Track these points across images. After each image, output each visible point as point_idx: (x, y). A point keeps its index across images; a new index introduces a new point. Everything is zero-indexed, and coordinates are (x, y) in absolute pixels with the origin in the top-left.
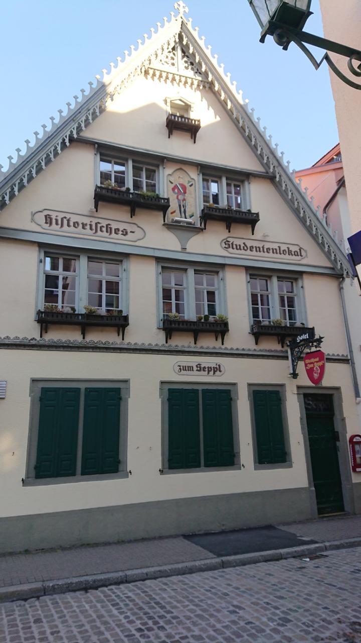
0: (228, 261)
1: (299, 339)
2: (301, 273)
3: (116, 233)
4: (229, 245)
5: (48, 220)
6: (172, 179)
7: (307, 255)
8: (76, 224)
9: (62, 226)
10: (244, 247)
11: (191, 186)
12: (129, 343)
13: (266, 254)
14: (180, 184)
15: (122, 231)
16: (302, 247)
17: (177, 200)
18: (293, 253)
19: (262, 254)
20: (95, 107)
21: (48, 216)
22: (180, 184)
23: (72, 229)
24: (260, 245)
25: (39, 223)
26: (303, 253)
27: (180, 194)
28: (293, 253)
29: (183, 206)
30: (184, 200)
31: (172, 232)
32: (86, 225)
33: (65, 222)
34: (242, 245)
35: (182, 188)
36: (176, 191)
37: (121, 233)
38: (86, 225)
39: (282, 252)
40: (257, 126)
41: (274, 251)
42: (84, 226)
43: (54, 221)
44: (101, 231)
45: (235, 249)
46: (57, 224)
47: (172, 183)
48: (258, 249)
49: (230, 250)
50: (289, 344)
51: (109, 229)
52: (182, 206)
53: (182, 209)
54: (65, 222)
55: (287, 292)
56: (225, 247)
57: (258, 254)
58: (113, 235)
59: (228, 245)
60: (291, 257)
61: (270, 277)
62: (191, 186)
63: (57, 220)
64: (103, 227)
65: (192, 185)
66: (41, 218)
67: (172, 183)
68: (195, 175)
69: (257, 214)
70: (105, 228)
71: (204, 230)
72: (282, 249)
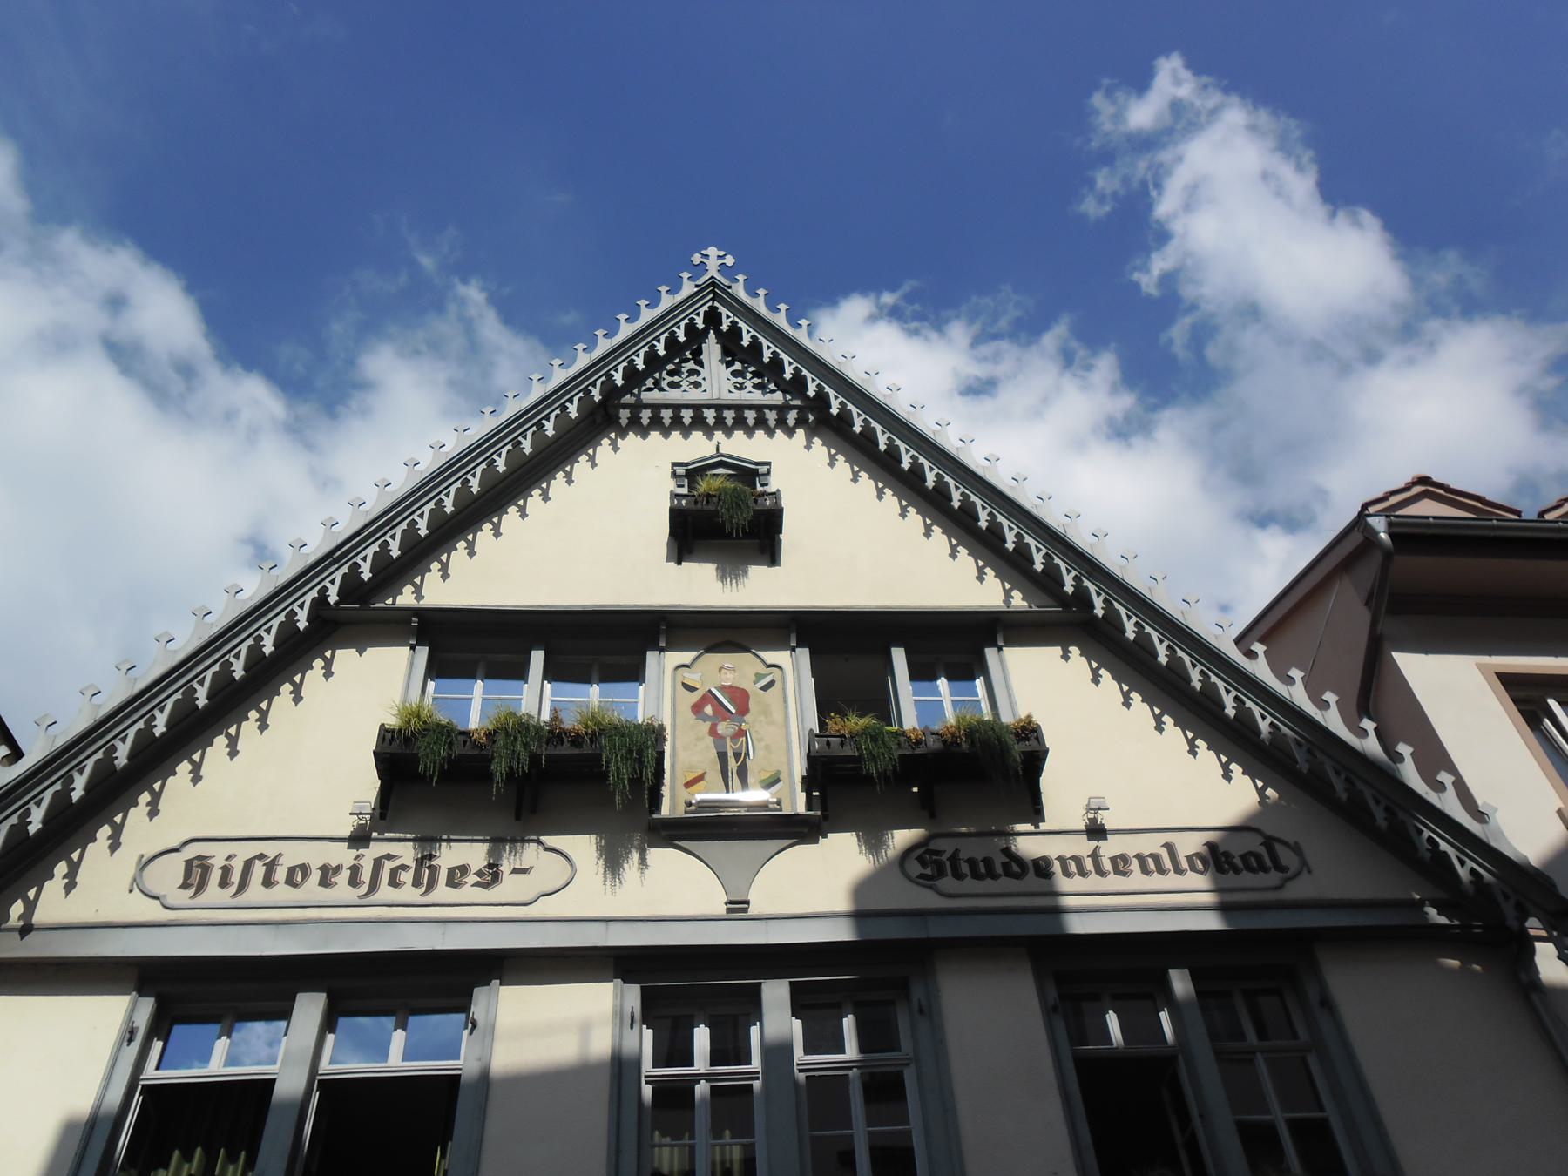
0: (938, 930)
3: (290, 881)
5: (196, 874)
6: (691, 677)
7: (1304, 864)
8: (298, 874)
9: (243, 885)
10: (1005, 866)
11: (765, 688)
13: (1113, 882)
14: (722, 689)
16: (1269, 831)
17: (710, 740)
18: (1238, 861)
20: (415, 517)
21: (196, 863)
22: (722, 689)
23: (282, 892)
25: (155, 892)
26: (1286, 857)
27: (724, 719)
28: (1238, 861)
29: (737, 755)
32: (337, 869)
33: (259, 870)
35: (732, 701)
36: (708, 710)
38: (337, 869)
39: (1184, 864)
42: (327, 875)
43: (216, 875)
44: (394, 882)
46: (224, 883)
49: (948, 883)
52: (730, 754)
54: (259, 870)
56: (922, 876)
62: (765, 688)
63: (226, 871)
64: (404, 867)
65: (772, 683)
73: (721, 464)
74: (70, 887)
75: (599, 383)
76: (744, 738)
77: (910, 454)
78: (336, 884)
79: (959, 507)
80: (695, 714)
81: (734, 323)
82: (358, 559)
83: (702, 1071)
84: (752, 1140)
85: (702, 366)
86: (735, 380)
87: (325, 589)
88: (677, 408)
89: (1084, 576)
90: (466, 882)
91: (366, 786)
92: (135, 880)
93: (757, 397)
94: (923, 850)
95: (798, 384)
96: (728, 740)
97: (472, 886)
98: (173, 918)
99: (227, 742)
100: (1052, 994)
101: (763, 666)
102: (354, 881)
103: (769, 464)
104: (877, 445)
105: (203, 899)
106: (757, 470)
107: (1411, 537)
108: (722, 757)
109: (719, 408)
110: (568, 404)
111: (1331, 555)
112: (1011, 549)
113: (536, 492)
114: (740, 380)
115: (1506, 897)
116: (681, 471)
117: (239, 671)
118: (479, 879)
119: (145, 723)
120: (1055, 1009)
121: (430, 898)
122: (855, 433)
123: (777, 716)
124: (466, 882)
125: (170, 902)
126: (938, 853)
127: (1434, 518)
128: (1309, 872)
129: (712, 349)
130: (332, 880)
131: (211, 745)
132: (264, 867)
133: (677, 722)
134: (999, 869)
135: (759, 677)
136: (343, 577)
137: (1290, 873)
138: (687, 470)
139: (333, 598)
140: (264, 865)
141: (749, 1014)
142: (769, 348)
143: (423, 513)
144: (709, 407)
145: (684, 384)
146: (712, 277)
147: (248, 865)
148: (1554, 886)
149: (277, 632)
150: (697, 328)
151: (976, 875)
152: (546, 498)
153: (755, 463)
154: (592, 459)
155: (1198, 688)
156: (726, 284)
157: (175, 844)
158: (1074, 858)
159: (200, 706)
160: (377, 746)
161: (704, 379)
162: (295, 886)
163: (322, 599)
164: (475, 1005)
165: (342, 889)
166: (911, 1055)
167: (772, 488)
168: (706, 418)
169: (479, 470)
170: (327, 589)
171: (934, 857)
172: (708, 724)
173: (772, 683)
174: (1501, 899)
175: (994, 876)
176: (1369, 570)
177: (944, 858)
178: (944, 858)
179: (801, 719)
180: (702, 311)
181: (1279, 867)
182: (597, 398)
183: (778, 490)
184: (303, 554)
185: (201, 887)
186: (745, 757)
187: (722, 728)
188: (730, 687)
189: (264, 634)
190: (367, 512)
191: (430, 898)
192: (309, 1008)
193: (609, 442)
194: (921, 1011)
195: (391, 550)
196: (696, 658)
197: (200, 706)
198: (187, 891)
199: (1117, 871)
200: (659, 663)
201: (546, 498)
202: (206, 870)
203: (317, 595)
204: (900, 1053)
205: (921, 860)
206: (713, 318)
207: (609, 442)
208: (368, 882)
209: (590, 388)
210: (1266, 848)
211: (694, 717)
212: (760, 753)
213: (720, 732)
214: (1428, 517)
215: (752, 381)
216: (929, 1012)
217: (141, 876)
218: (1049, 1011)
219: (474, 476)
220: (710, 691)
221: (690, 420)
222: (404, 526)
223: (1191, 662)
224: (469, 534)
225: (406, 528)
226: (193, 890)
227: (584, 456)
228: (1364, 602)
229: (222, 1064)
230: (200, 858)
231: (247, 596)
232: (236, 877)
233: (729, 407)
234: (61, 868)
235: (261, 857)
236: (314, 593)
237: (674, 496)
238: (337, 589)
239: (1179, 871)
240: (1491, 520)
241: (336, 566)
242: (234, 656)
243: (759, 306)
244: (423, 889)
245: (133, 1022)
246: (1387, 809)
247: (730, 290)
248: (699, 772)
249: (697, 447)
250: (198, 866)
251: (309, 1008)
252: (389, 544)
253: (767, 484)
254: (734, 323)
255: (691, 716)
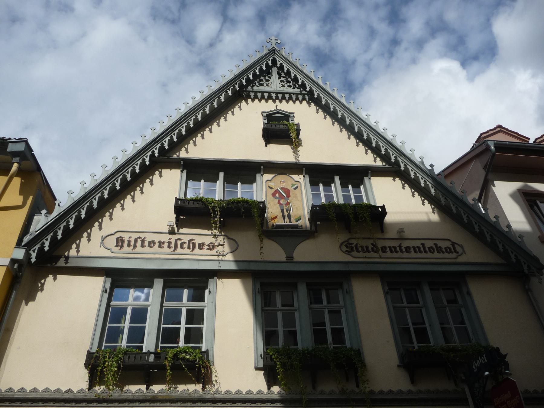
0: (352, 268)
1: (476, 365)
2: (463, 275)
3: (149, 246)
4: (352, 248)
5: (120, 242)
6: (271, 184)
7: (464, 251)
8: (151, 244)
9: (135, 247)
10: (372, 249)
11: (295, 189)
12: (217, 392)
13: (406, 255)
14: (281, 188)
15: (208, 245)
16: (454, 240)
17: (278, 205)
18: (444, 250)
19: (399, 255)
20: (181, 128)
21: (119, 239)
22: (281, 188)
23: (147, 249)
24: (396, 244)
25: (108, 247)
26: (458, 249)
27: (282, 199)
28: (444, 250)
29: (287, 211)
30: (288, 203)
31: (273, 240)
32: (164, 243)
33: (139, 242)
34: (371, 247)
35: (285, 192)
36: (277, 195)
37: (206, 247)
38: (164, 243)
39: (427, 250)
40: (367, 122)
41: (417, 250)
42: (161, 244)
43: (126, 243)
44: (182, 247)
45: (399, 253)
46: (129, 245)
47: (271, 188)
48: (393, 249)
49: (355, 253)
50: (463, 378)
51: (191, 245)
52: (285, 210)
53: (286, 214)
54: (139, 242)
55: (283, 306)
56: (346, 251)
57: (395, 255)
58: (197, 251)
59: (349, 248)
60: (441, 255)
61: (295, 286)
62: (295, 189)
63: (129, 242)
64: (185, 243)
65: (297, 187)
66: (111, 242)
67: (271, 188)
68: (302, 180)
69: (383, 207)
70: (187, 244)
71: (316, 234)
72: (427, 246)
73: (278, 113)
74: (89, 240)
75: (238, 83)
76: (289, 205)
77: (341, 112)
78: (164, 247)
79: (357, 131)
80: (273, 197)
81: (281, 64)
82: (163, 142)
83: (279, 308)
84: (296, 329)
85: (271, 79)
86: (281, 84)
87: (154, 151)
88: (263, 93)
89: (398, 156)
90: (204, 248)
91: (172, 217)
92: (101, 243)
93: (290, 90)
94: (347, 243)
95: (303, 86)
96: (284, 205)
97: (206, 249)
98: (114, 256)
99: (131, 197)
100: (387, 288)
101: (294, 181)
102: (169, 247)
103: (294, 113)
104: (330, 109)
105: (122, 250)
106: (290, 115)
107: (501, 147)
108: (282, 211)
109: (277, 93)
110: (228, 90)
111: (469, 155)
112: (374, 146)
113: (215, 124)
114: (283, 84)
115: (525, 263)
116: (265, 115)
117: (95, 205)
118: (208, 247)
119: (101, 194)
120: (387, 293)
121: (193, 253)
122: (323, 104)
123: (299, 198)
124: (204, 248)
125: (113, 251)
126: (352, 244)
127: (508, 142)
128: (465, 254)
129: (275, 70)
130: (163, 246)
131: (126, 198)
132: (141, 241)
133: (267, 199)
134: (370, 250)
135: (293, 185)
136: (99, 197)
137: (459, 254)
138: (267, 114)
139: (157, 155)
140: (141, 240)
141: (276, 291)
142: (293, 73)
143: (138, 163)
144: (273, 93)
145: (265, 84)
146: (273, 47)
147: (136, 240)
148: (539, 260)
149: (75, 219)
150: (250, 79)
151: (363, 251)
152: (211, 131)
153: (289, 113)
154: (240, 107)
155: (434, 195)
156: (278, 50)
157: (112, 233)
158: (393, 247)
159: (106, 198)
160: (175, 204)
161: (271, 83)
162: (151, 247)
163: (153, 155)
164: (210, 286)
165: (165, 249)
166: (343, 305)
167: (296, 122)
168: (272, 97)
169: (200, 113)
170: (135, 168)
171: (350, 245)
172: (278, 200)
173: (297, 187)
174: (523, 264)
175: (369, 252)
176: (486, 158)
177: (353, 246)
178: (353, 246)
179: (307, 200)
180: (270, 59)
181: (456, 252)
182: (238, 89)
183: (299, 123)
184: (145, 139)
185: (122, 247)
186: (290, 211)
187: (282, 201)
188: (284, 188)
189: (135, 166)
190: (165, 126)
191: (193, 253)
192: (159, 284)
193: (217, 124)
194: (347, 292)
195: (190, 125)
196: (274, 177)
197: (106, 198)
198: (118, 248)
199: (430, 252)
200: (261, 179)
201: (211, 131)
202: (123, 241)
203: (151, 153)
204: (339, 305)
205: (346, 246)
206: (274, 62)
207: (217, 124)
208: (175, 246)
209: (235, 85)
210: (452, 246)
211: (273, 197)
212: (295, 210)
213: (281, 203)
214: (507, 142)
215: (287, 84)
216: (349, 293)
217: (103, 243)
218: (386, 294)
219: (199, 114)
220: (277, 189)
221: (267, 97)
222: (177, 131)
223: (432, 186)
224: (186, 145)
225: (178, 131)
226: (120, 247)
227: (223, 117)
228: (483, 168)
229: (133, 301)
230: (120, 237)
231: (129, 153)
232: (132, 244)
233: (280, 93)
234: (85, 235)
235: (140, 238)
236: (150, 153)
237: (264, 124)
238: (119, 184)
239: (426, 252)
240: (526, 143)
241: (157, 144)
242: (126, 173)
243: (290, 58)
244: (191, 250)
245: (106, 287)
246: (490, 235)
247: (279, 52)
248: (275, 215)
249: (270, 106)
250: (120, 240)
251: (159, 284)
252: (181, 130)
253: (293, 120)
254: (281, 64)
255: (271, 197)
